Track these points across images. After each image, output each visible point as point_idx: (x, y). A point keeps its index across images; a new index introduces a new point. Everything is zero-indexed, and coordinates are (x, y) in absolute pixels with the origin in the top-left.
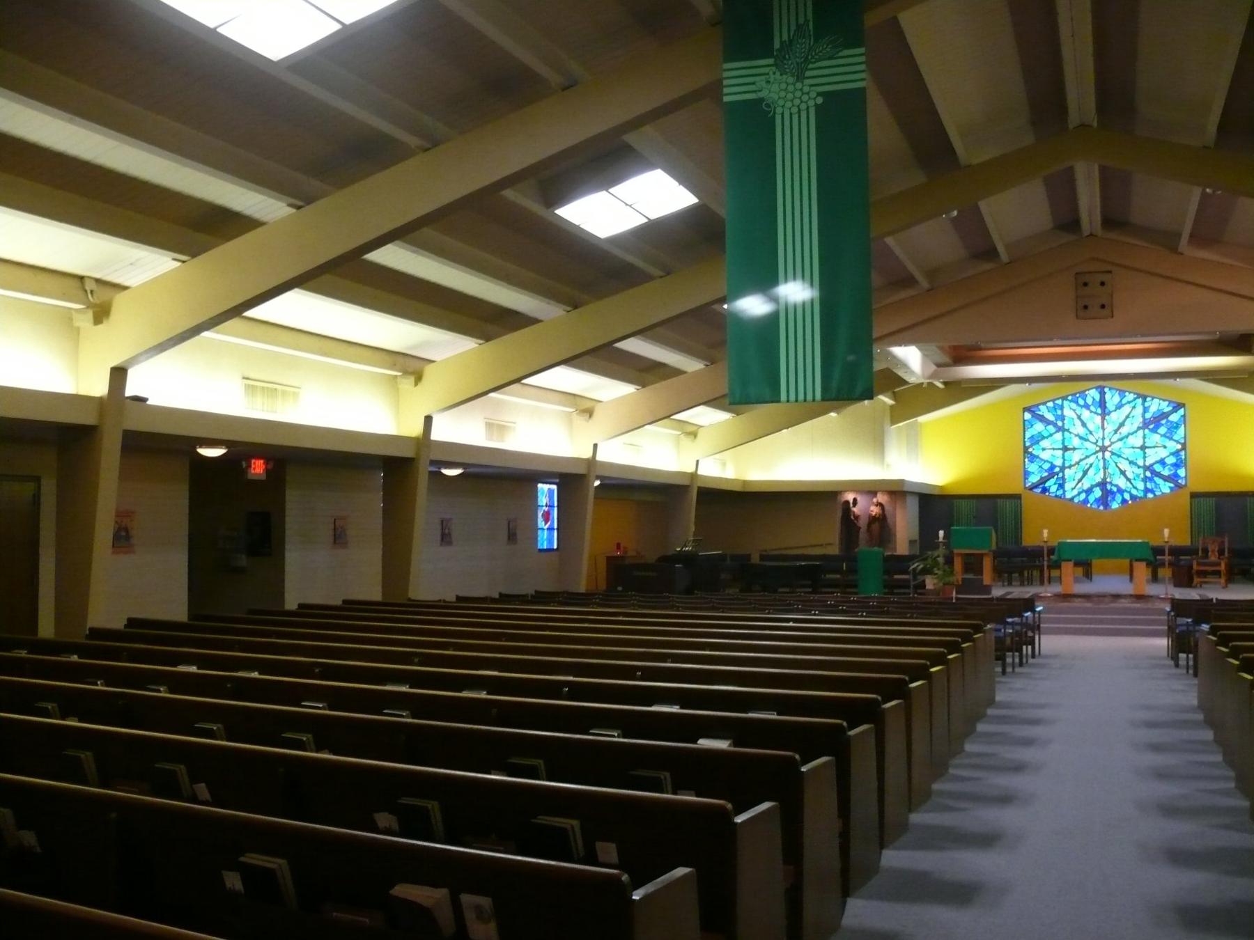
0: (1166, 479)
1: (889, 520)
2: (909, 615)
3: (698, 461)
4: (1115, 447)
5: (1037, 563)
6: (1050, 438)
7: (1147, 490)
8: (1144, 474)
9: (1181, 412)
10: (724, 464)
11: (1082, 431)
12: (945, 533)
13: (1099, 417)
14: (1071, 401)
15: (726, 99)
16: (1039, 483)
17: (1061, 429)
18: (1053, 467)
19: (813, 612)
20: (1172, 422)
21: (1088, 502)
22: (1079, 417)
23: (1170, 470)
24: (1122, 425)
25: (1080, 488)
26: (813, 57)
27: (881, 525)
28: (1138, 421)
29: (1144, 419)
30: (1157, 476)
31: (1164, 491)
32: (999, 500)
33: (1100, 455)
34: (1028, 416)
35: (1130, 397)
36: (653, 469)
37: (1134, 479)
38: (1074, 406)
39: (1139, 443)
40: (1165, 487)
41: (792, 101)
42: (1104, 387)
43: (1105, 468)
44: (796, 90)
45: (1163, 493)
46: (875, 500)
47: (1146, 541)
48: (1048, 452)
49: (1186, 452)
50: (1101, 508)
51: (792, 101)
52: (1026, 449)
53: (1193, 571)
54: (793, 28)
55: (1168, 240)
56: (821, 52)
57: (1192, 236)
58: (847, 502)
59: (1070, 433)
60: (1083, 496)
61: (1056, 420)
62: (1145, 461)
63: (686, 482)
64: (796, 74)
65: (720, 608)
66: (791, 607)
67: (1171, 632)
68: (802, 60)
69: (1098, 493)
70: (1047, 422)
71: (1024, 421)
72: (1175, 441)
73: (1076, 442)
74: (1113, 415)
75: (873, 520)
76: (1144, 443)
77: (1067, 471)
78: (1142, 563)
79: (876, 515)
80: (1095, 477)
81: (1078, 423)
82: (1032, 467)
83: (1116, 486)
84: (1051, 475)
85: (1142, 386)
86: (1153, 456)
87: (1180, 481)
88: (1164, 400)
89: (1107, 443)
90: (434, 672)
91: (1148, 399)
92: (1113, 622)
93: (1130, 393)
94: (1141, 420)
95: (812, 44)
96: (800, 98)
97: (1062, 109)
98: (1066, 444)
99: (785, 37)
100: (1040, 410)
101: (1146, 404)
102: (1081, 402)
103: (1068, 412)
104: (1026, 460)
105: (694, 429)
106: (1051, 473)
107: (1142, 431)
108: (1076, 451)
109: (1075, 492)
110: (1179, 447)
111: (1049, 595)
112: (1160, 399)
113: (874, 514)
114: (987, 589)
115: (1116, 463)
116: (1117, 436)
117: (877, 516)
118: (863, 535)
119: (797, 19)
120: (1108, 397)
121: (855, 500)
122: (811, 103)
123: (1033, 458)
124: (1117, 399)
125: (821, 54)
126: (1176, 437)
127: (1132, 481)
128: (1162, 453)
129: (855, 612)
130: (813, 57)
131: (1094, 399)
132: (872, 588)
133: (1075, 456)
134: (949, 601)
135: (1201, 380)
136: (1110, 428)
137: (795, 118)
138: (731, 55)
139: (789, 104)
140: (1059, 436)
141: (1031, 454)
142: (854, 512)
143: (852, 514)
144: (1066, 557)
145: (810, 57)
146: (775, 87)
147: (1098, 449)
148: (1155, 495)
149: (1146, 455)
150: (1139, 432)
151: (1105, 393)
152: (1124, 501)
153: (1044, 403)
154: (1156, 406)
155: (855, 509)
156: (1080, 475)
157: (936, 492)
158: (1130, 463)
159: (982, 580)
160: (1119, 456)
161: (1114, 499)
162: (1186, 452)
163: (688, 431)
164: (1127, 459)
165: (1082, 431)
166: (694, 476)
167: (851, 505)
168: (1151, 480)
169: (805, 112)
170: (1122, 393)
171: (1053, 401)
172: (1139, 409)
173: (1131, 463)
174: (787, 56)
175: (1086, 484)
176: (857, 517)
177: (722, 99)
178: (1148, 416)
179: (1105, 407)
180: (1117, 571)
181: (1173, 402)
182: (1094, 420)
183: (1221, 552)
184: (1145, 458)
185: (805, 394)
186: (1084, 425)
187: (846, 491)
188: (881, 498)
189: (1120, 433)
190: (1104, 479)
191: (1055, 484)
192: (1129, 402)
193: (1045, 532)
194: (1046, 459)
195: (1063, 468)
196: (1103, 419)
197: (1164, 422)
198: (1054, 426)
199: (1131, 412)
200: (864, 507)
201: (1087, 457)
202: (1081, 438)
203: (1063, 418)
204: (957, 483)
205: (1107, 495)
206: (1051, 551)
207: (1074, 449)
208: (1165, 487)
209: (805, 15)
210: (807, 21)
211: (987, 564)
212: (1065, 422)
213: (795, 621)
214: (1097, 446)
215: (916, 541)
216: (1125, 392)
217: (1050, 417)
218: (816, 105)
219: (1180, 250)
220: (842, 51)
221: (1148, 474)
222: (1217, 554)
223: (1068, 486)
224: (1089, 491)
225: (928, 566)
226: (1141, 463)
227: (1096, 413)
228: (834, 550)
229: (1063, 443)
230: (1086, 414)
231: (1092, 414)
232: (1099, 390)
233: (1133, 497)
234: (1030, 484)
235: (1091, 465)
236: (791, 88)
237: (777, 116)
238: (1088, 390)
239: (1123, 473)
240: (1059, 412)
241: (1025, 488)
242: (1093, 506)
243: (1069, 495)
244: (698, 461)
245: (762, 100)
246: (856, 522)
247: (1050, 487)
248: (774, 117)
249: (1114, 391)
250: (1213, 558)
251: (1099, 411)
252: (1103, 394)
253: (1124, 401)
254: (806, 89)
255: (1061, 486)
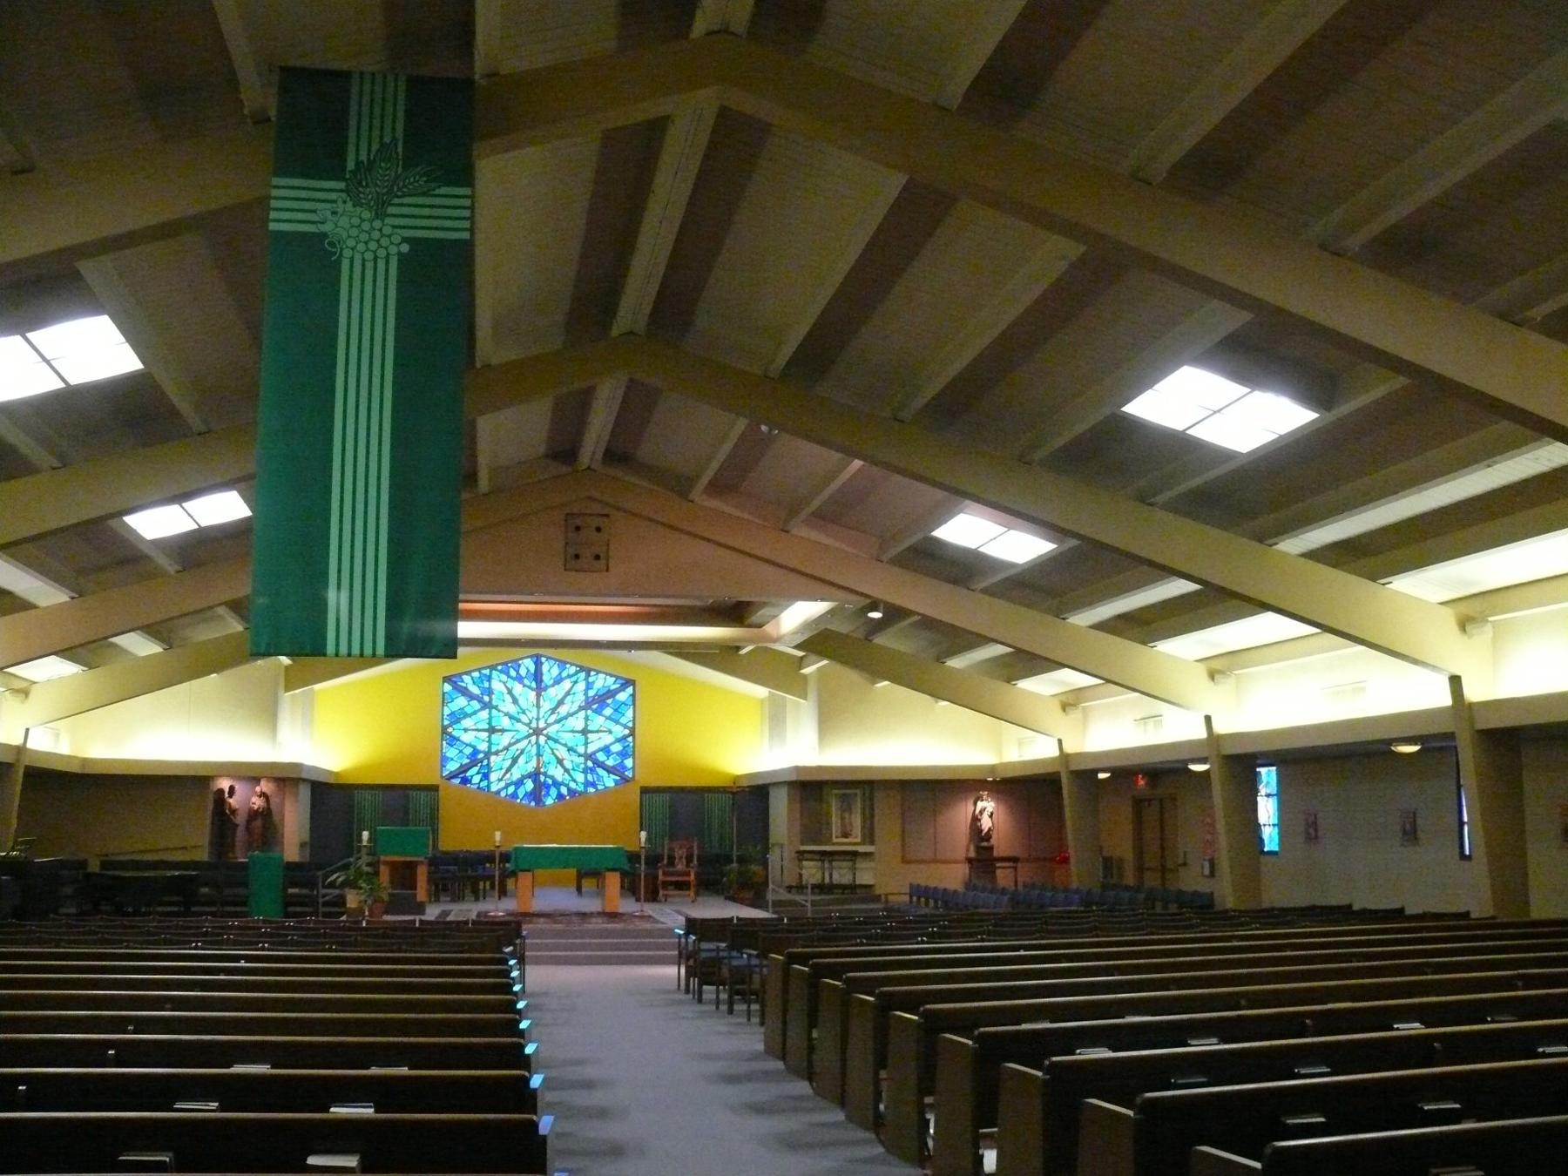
0: (610, 770)
1: (276, 818)
2: (395, 948)
3: (27, 730)
4: (552, 730)
5: (470, 872)
6: (474, 717)
7: (587, 784)
8: (585, 763)
9: (630, 690)
10: (57, 735)
11: (513, 709)
12: (370, 834)
13: (534, 693)
14: (501, 671)
15: (273, 226)
16: (458, 772)
17: (487, 706)
18: (476, 752)
19: (260, 945)
20: (618, 701)
21: (518, 798)
22: (510, 692)
23: (615, 760)
24: (561, 703)
25: (509, 779)
26: (399, 189)
27: (265, 823)
28: (579, 699)
29: (587, 697)
31: (607, 785)
32: (411, 792)
33: (534, 739)
34: (448, 687)
35: (573, 669)
36: (1282, 729)
37: (573, 769)
38: (504, 678)
39: (580, 725)
40: (609, 781)
41: (366, 243)
42: (542, 656)
43: (539, 755)
44: (373, 228)
45: (606, 788)
46: (258, 789)
47: (620, 846)
48: (471, 734)
49: (634, 738)
50: (533, 804)
51: (366, 243)
52: (444, 730)
53: (659, 882)
54: (375, 147)
55: (680, 485)
56: (411, 184)
57: (710, 483)
58: (221, 791)
59: (499, 711)
60: (511, 789)
61: (482, 694)
62: (586, 748)
63: (9, 759)
64: (375, 207)
65: (122, 941)
66: (220, 938)
67: (685, 956)
68: (385, 190)
69: (529, 785)
70: (472, 697)
71: (444, 694)
72: (622, 725)
73: (505, 723)
75: (254, 815)
76: (586, 725)
77: (493, 758)
78: (615, 873)
79: (259, 808)
80: (525, 766)
81: (508, 698)
82: (451, 752)
83: (552, 777)
84: (473, 763)
85: (586, 657)
86: (596, 742)
87: (626, 773)
88: (611, 676)
89: (542, 725)
90: (1498, 1127)
91: (592, 673)
92: (602, 947)
93: (572, 665)
94: (584, 698)
95: (399, 172)
96: (378, 241)
97: (609, 308)
98: (494, 724)
99: (363, 157)
100: (463, 681)
101: (591, 679)
102: (513, 673)
103: (497, 685)
104: (444, 742)
105: (23, 685)
106: (474, 760)
107: (584, 711)
108: (506, 733)
109: (502, 784)
110: (627, 732)
111: (501, 914)
112: (607, 674)
113: (256, 807)
114: (420, 909)
115: (552, 750)
116: (553, 718)
117: (261, 810)
118: (240, 833)
119: (381, 138)
120: (545, 668)
121: (232, 789)
122: (393, 250)
123: (453, 740)
124: (555, 671)
125: (411, 187)
126: (623, 720)
127: (572, 772)
128: (607, 739)
129: (251, 943)
130: (399, 189)
131: (528, 671)
132: (265, 908)
133: (502, 740)
134: (412, 926)
135: (666, 652)
136: (546, 706)
137: (370, 265)
138: (285, 167)
139: (361, 247)
140: (484, 714)
141: (450, 735)
142: (230, 804)
143: (228, 807)
144: (522, 867)
145: (395, 189)
146: (344, 221)
147: (531, 731)
148: (597, 789)
149: (589, 741)
150: (580, 713)
151: (542, 664)
152: (560, 797)
154: (601, 682)
155: (231, 801)
157: (332, 781)
158: (568, 750)
159: (415, 895)
160: (556, 741)
161: (548, 794)
162: (634, 738)
163: (15, 687)
164: (565, 745)
165: (513, 709)
166: (20, 750)
167: (227, 795)
168: (592, 770)
169: (384, 261)
170: (562, 664)
171: (479, 670)
172: (581, 686)
173: (570, 749)
174: (364, 184)
175: (516, 774)
176: (234, 812)
177: (268, 226)
178: (591, 693)
179: (542, 681)
180: (557, 883)
181: (622, 678)
182: (527, 696)
183: (689, 859)
184: (586, 744)
185: (337, 645)
186: (515, 701)
187: (220, 776)
188: (265, 786)
189: (558, 713)
190: (538, 768)
191: (478, 773)
192: (569, 676)
193: (498, 836)
194: (468, 742)
195: (488, 754)
196: (538, 696)
197: (609, 701)
199: (572, 687)
200: (244, 799)
201: (518, 741)
202: (511, 717)
203: (490, 692)
204: (357, 769)
205: (540, 787)
206: (505, 857)
207: (503, 731)
208: (609, 781)
209: (394, 129)
210: (394, 139)
211: (422, 874)
212: (493, 697)
213: (248, 959)
214: (530, 728)
215: (306, 843)
216: (566, 663)
217: (475, 690)
218: (400, 254)
219: (691, 497)
220: (439, 187)
221: (590, 764)
222: (684, 861)
223: (494, 777)
224: (519, 783)
225: (352, 878)
227: (529, 687)
228: (203, 855)
229: (489, 724)
230: (518, 688)
231: (527, 689)
233: (572, 792)
234: (447, 773)
235: (522, 752)
236: (366, 226)
237: (343, 259)
238: (521, 659)
239: (560, 762)
240: (486, 685)
242: (524, 802)
243: (494, 788)
244: (27, 730)
245: (324, 235)
246: (232, 817)
247: (472, 777)
248: (338, 262)
249: (552, 662)
250: (680, 867)
251: (534, 685)
252: (538, 664)
253: (564, 674)
254: (387, 230)
255: (486, 776)
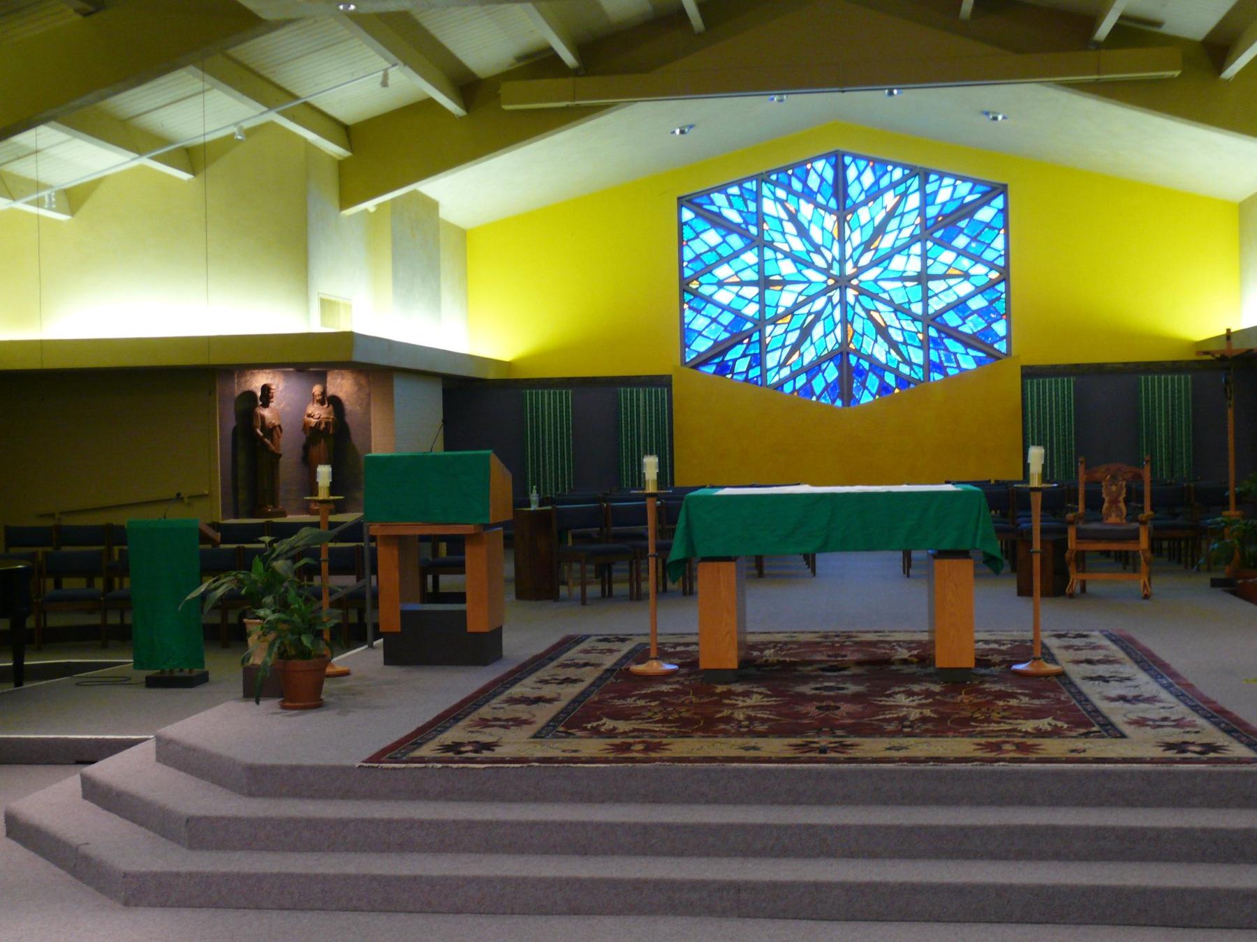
11: (798, 245)
17: (758, 243)
29: (925, 219)
30: (949, 336)
50: (839, 403)
60: (801, 380)
74: (864, 214)
81: (790, 228)
91: (933, 177)
100: (712, 203)
101: (930, 188)
109: (785, 372)
140: (751, 257)
151: (845, 167)
153: (722, 189)
156: (792, 338)
165: (798, 245)
171: (739, 183)
172: (914, 201)
175: (809, 354)
179: (846, 196)
186: (803, 232)
191: (744, 355)
198: (741, 236)
203: (760, 218)
223: (772, 360)
224: (813, 369)
226: (917, 309)
230: (806, 211)
232: (833, 160)
240: (752, 207)
241: (684, 363)
243: (772, 378)
249: (862, 163)
251: (833, 204)
253: (885, 182)
255: (758, 360)
